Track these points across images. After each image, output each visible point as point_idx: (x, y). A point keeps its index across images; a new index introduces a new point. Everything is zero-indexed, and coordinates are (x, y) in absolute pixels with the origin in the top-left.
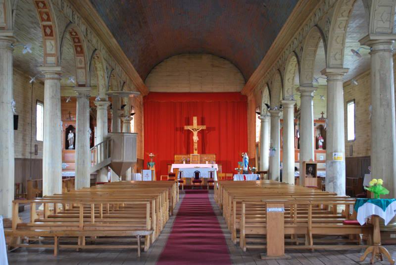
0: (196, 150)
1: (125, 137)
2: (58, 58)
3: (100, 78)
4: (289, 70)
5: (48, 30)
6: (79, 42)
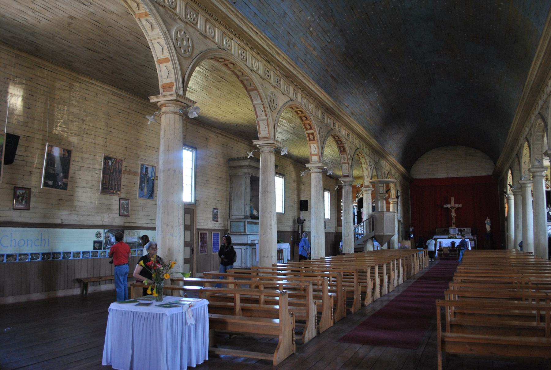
0: (454, 224)
1: (385, 215)
2: (320, 157)
3: (365, 169)
4: (524, 154)
5: (311, 137)
6: (341, 143)
